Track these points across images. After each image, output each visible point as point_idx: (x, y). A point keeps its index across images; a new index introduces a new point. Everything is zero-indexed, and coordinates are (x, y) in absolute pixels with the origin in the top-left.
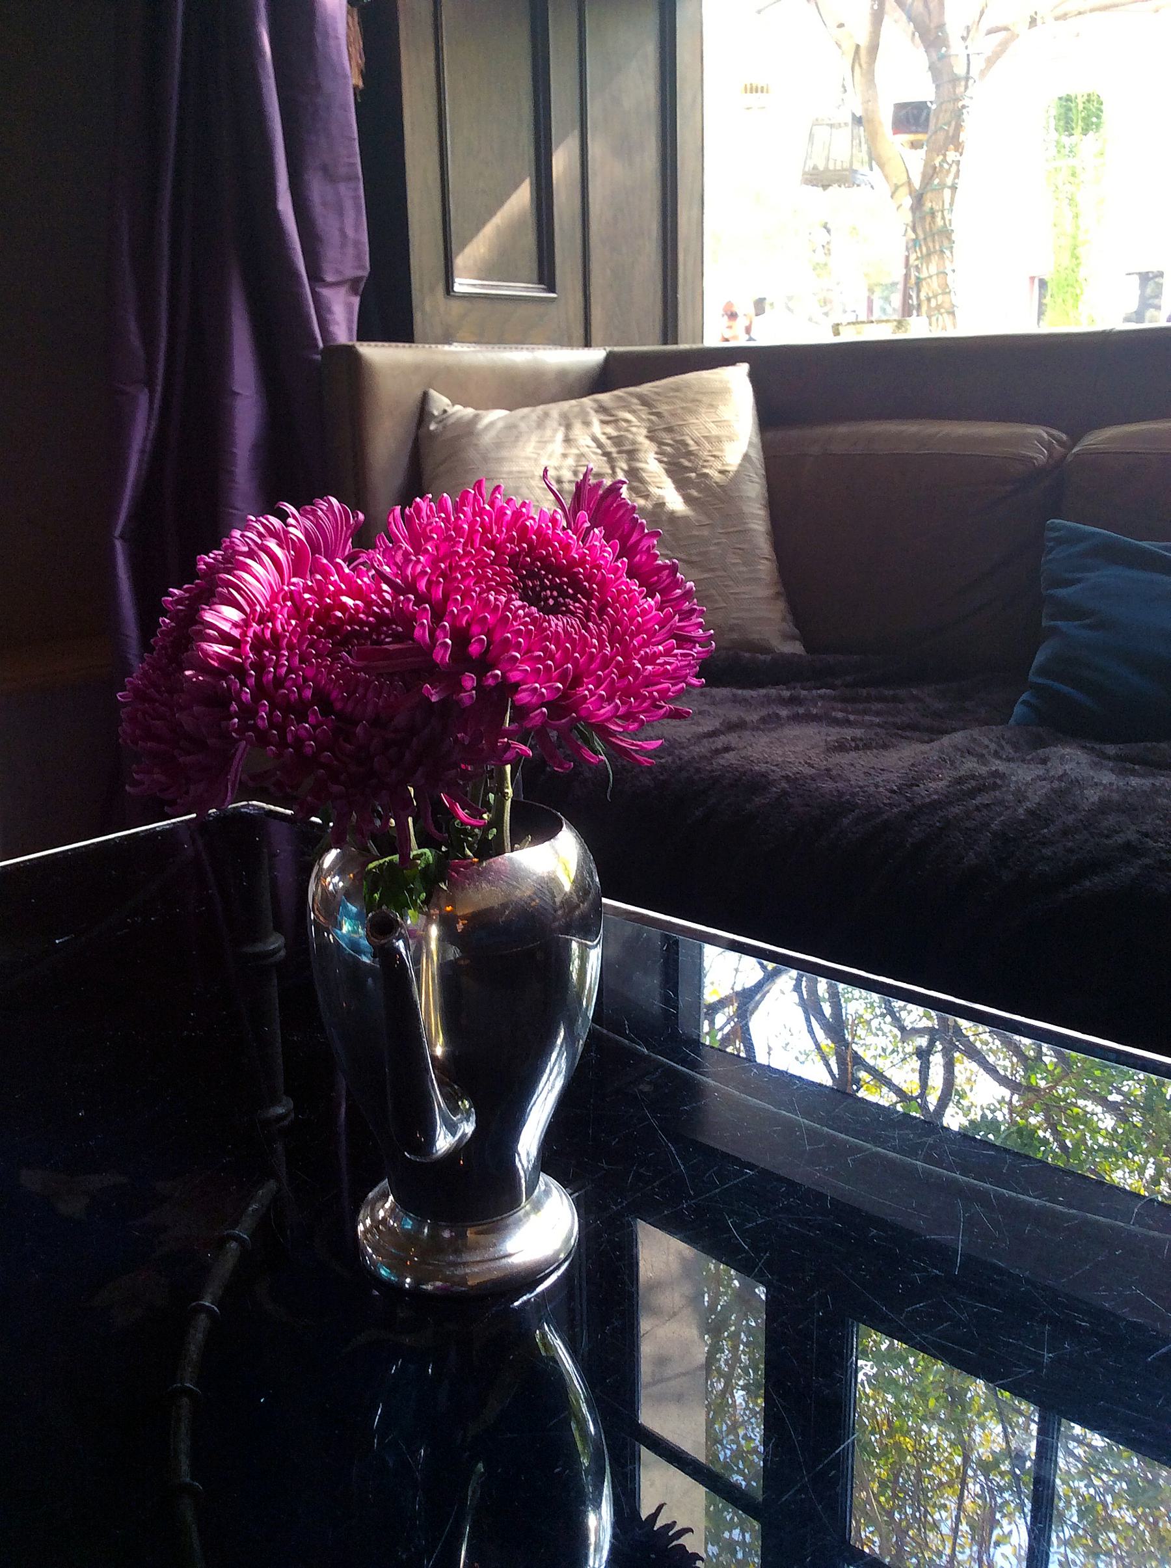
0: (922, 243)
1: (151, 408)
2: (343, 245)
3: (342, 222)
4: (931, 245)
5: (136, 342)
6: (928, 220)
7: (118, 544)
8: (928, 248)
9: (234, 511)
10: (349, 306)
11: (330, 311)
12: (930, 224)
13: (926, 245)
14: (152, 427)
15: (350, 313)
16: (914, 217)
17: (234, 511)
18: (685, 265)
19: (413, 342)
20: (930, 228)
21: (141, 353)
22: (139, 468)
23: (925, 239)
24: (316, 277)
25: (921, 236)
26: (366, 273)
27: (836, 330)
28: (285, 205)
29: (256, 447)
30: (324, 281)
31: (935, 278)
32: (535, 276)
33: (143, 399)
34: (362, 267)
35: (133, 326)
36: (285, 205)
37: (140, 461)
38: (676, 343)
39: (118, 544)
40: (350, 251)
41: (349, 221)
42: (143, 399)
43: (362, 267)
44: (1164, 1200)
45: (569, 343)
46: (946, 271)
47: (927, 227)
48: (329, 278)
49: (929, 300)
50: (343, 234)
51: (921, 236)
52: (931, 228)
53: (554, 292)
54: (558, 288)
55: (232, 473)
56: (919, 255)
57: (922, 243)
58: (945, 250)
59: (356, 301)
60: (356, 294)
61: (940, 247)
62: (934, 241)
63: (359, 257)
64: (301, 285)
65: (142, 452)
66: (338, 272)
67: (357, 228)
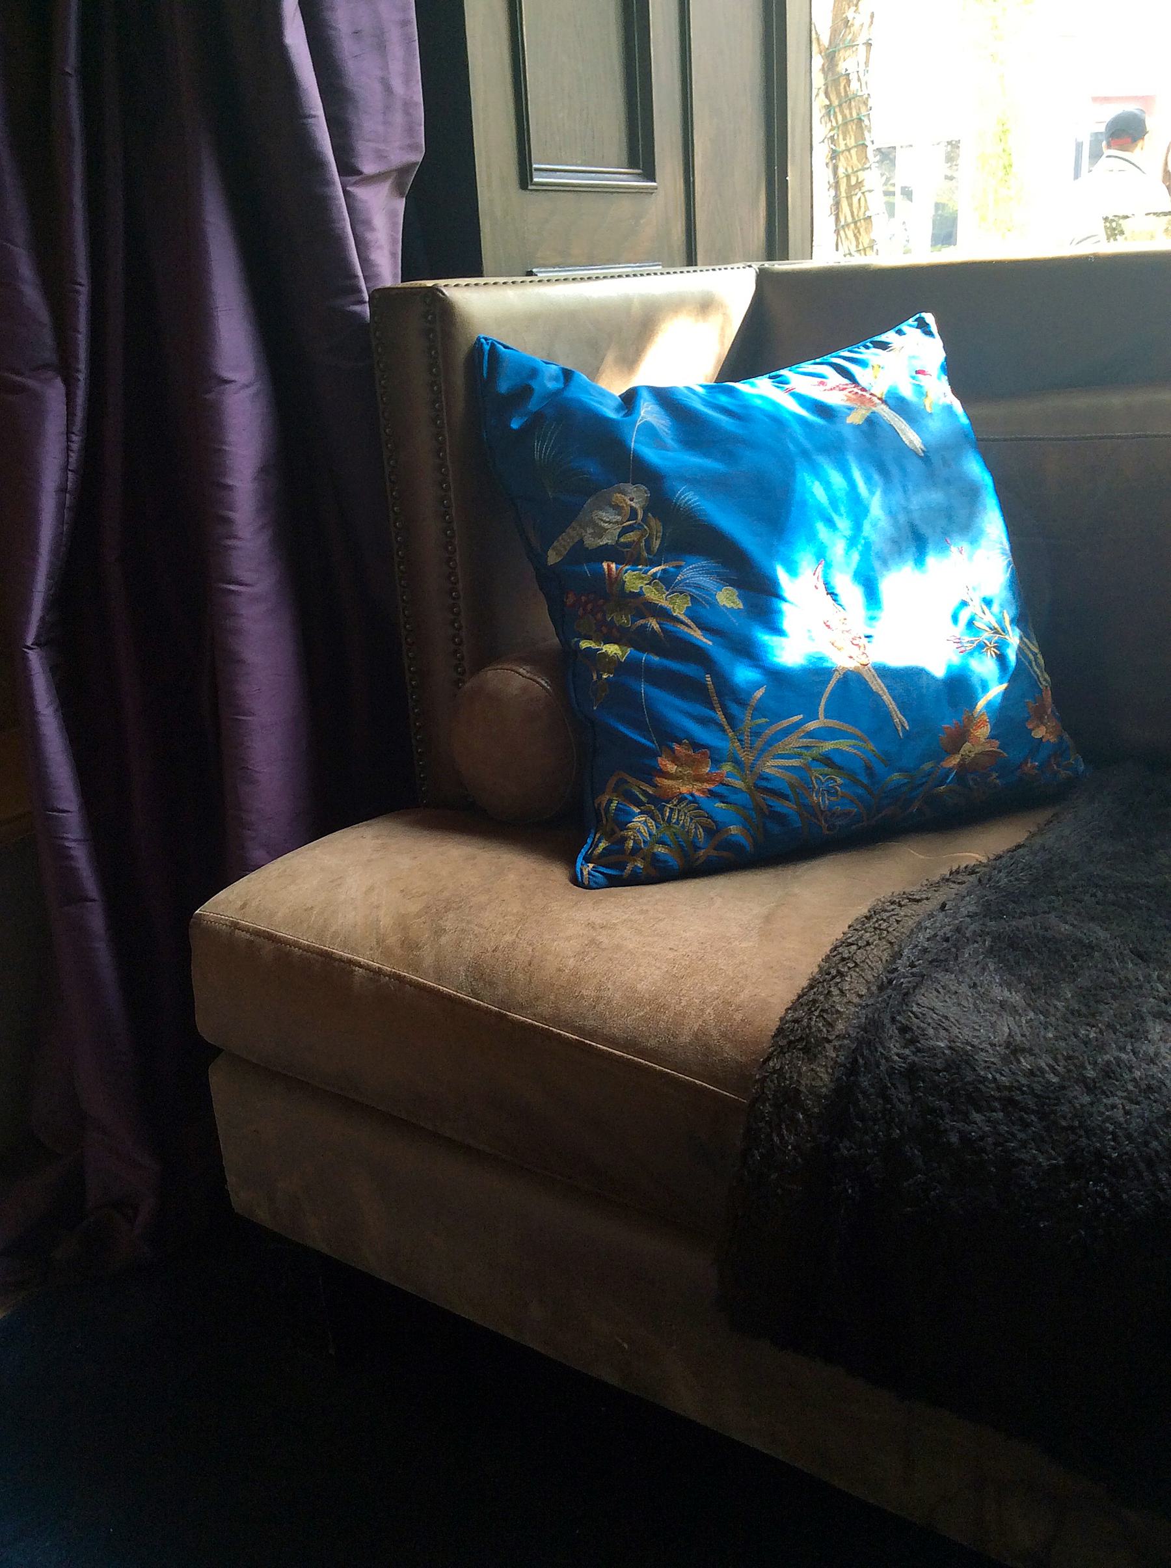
0: (837, 110)
1: (70, 414)
2: (387, 109)
3: (385, 67)
4: (847, 112)
5: (31, 294)
6: (843, 83)
7: (35, 659)
8: (844, 117)
9: (232, 587)
10: (392, 214)
11: (368, 223)
12: (845, 86)
13: (842, 112)
14: (75, 446)
15: (395, 224)
16: (826, 79)
17: (232, 587)
18: (793, 137)
19: (479, 273)
20: (846, 91)
21: (44, 316)
22: (60, 519)
23: (840, 105)
24: (348, 169)
25: (836, 103)
26: (418, 157)
27: (1113, 230)
28: (295, 37)
29: (264, 471)
30: (359, 173)
31: (853, 152)
32: (624, 156)
33: (54, 394)
34: (413, 147)
35: (26, 269)
36: (295, 37)
37: (61, 506)
38: (785, 257)
39: (35, 659)
40: (398, 118)
41: (396, 66)
42: (54, 394)
43: (413, 147)
44: (1042, 1093)
45: (669, 263)
46: (866, 143)
47: (842, 91)
48: (369, 168)
49: (848, 177)
50: (388, 89)
51: (836, 103)
52: (846, 91)
53: (655, 182)
54: (657, 179)
55: (228, 521)
56: (834, 124)
57: (837, 110)
58: (863, 118)
59: (400, 205)
60: (401, 195)
61: (858, 115)
62: (850, 109)
63: (410, 130)
64: (328, 183)
65: (62, 490)
66: (380, 156)
67: (407, 81)
